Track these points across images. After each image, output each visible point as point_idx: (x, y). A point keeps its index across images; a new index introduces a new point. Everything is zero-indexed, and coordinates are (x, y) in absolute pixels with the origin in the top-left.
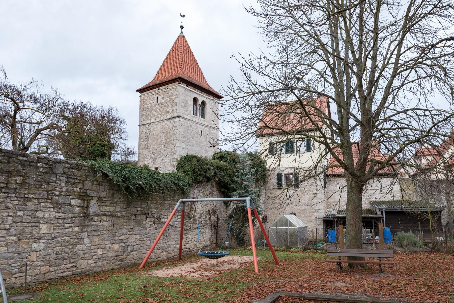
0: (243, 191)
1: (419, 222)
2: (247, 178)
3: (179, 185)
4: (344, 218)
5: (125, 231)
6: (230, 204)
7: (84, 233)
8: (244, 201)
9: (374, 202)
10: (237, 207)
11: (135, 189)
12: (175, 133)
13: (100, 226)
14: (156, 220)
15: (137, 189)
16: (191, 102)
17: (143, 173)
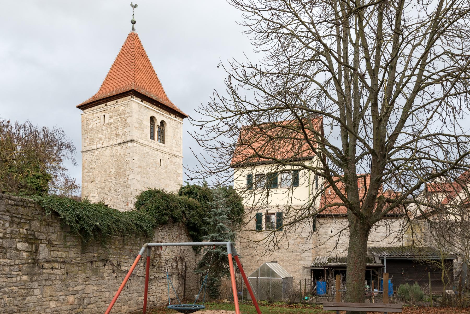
0: (217, 235)
1: (429, 273)
2: (222, 218)
3: (141, 227)
4: (345, 267)
5: (80, 281)
6: (200, 250)
7: (34, 283)
8: (226, 245)
9: (373, 248)
10: (209, 253)
11: (91, 231)
12: (128, 162)
13: (52, 274)
14: (115, 268)
15: (93, 231)
16: (147, 123)
17: (99, 211)
